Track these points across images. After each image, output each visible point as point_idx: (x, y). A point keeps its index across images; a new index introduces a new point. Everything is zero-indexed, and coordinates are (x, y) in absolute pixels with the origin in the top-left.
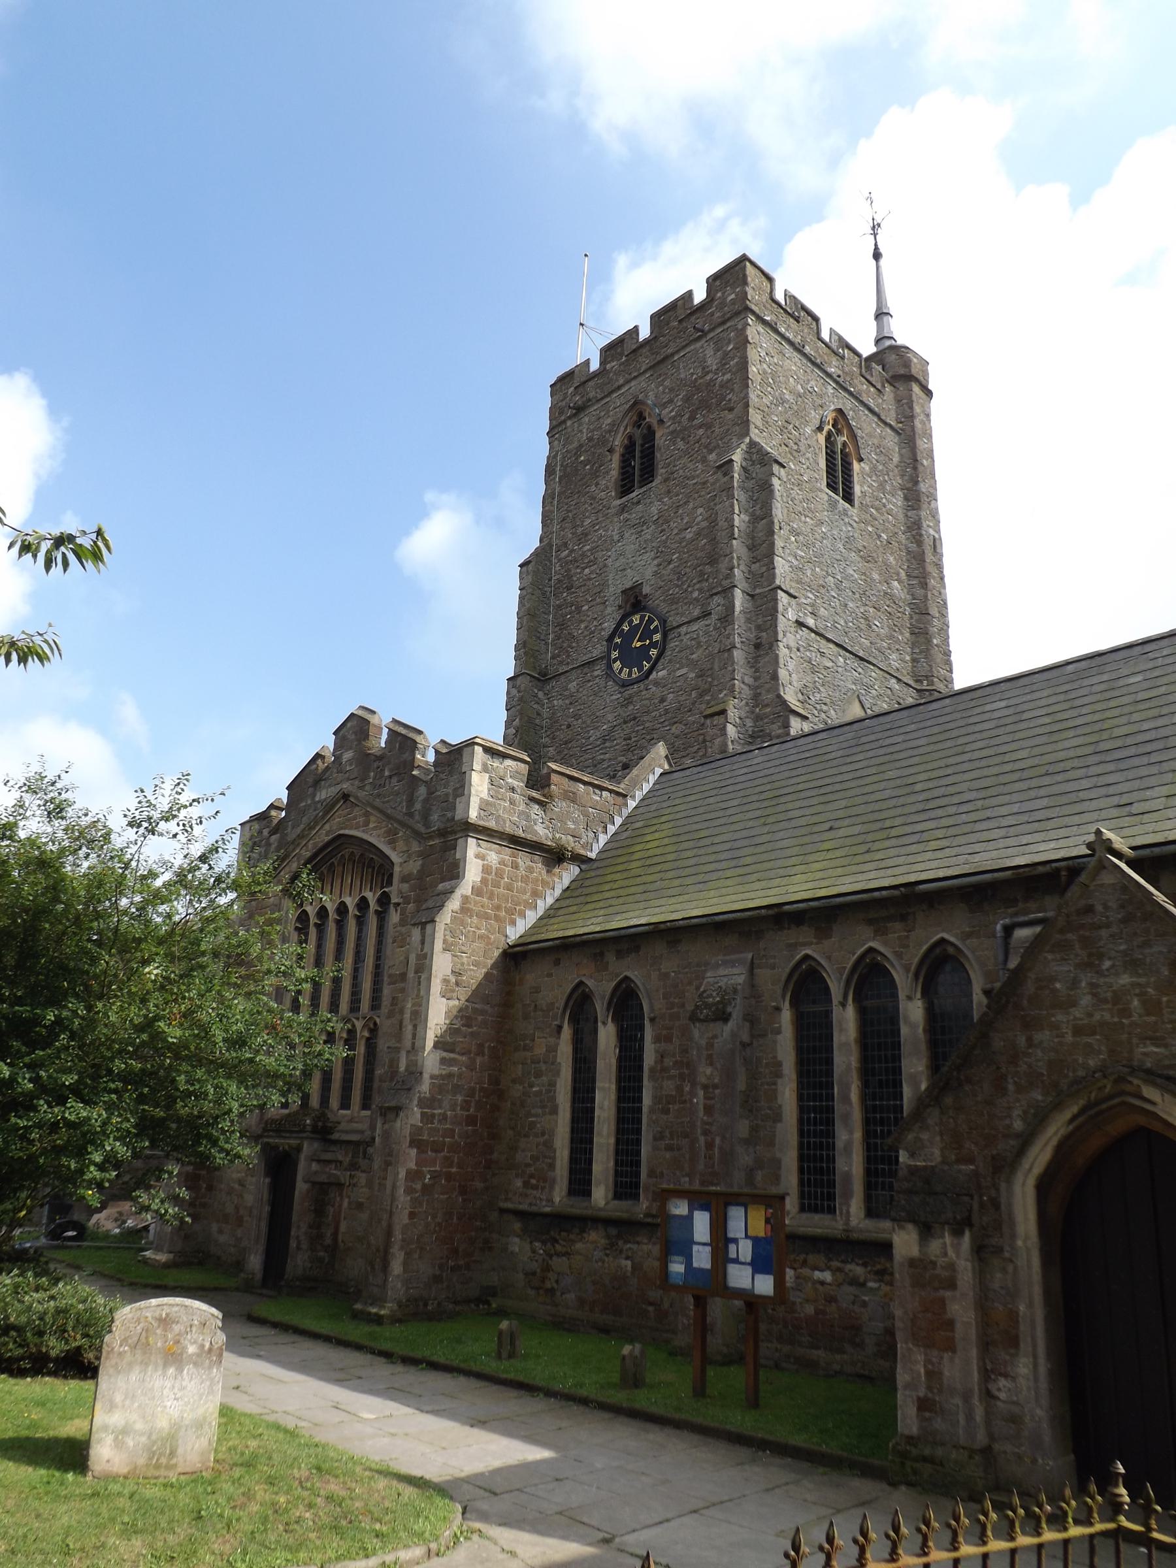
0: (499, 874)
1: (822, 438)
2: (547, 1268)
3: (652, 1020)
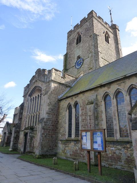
0: (57, 88)
1: (104, 34)
2: (65, 149)
3: (81, 107)
